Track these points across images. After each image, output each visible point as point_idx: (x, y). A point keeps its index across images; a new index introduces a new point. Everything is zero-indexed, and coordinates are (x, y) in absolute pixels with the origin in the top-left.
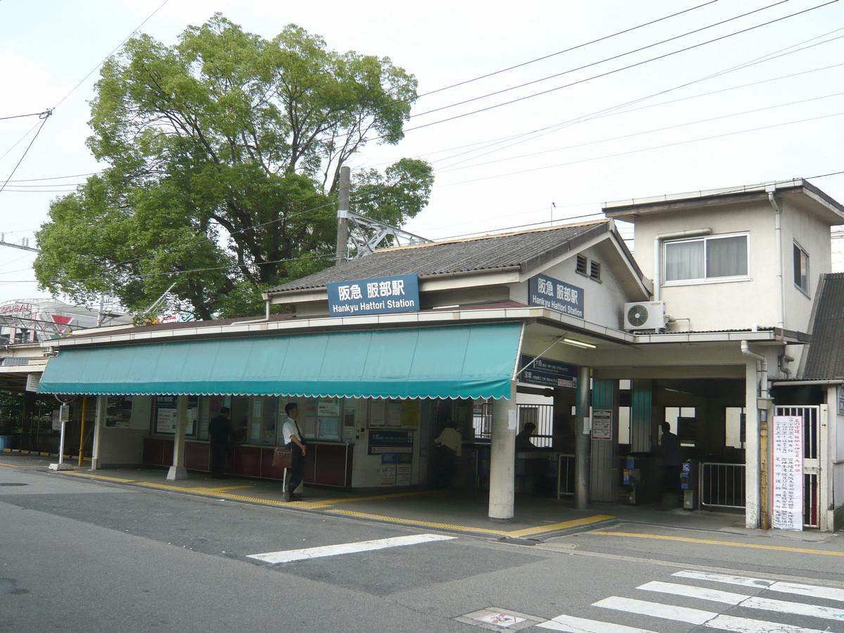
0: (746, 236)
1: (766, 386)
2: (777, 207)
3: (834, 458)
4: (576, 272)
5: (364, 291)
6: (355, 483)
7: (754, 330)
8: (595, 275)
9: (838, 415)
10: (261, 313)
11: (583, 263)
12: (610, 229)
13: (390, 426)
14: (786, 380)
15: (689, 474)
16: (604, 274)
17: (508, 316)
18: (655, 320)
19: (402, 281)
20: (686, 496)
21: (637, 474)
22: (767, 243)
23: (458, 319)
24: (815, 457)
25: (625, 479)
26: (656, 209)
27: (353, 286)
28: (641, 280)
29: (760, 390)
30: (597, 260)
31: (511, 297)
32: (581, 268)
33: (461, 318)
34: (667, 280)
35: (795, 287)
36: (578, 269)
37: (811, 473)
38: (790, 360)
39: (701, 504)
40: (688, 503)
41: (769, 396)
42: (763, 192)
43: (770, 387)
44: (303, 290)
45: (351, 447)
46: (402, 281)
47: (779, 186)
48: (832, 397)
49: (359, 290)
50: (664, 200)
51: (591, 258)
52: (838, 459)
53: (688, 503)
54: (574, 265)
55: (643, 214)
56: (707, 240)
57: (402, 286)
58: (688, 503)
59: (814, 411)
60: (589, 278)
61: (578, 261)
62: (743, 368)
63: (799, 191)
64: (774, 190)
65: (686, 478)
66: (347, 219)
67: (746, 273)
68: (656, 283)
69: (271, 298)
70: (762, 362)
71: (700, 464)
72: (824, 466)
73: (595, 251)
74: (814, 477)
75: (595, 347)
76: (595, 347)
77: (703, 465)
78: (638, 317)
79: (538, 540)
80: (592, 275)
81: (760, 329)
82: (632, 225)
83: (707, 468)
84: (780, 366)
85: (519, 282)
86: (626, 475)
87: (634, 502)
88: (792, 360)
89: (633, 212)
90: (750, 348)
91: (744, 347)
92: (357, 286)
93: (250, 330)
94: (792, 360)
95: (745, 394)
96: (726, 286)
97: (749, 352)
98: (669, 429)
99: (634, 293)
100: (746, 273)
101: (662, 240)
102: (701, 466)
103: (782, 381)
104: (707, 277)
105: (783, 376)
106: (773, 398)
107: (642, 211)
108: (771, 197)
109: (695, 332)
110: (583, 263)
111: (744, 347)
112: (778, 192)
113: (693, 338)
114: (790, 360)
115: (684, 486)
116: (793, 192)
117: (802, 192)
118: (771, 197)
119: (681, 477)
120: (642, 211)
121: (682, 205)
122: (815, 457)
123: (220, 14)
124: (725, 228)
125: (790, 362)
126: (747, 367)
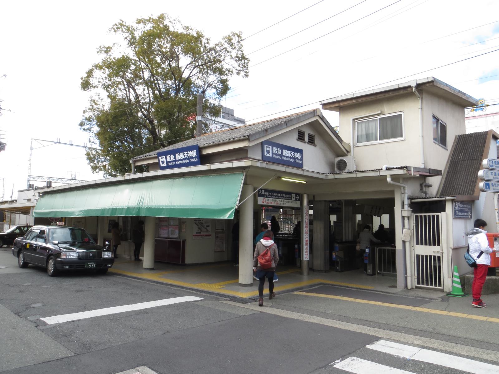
0: (401, 114)
1: (406, 202)
2: (419, 96)
3: (451, 246)
4: (297, 140)
5: (175, 157)
6: (188, 261)
7: (384, 169)
8: (312, 141)
9: (453, 218)
10: (130, 170)
11: (303, 135)
12: (318, 114)
13: (218, 230)
14: (425, 198)
15: (369, 254)
16: (317, 140)
17: (234, 166)
18: (351, 166)
19: (195, 151)
20: (368, 267)
21: (341, 254)
22: (415, 117)
23: (210, 169)
24: (439, 245)
25: (333, 257)
26: (348, 102)
27: (172, 155)
28: (341, 144)
29: (403, 205)
30: (312, 133)
31: (248, 155)
32: (301, 137)
33: (212, 168)
34: (358, 143)
35: (434, 142)
36: (298, 138)
37: (437, 255)
38: (429, 186)
39: (377, 271)
40: (369, 271)
41: (409, 208)
42: (409, 87)
43: (409, 203)
44: (148, 157)
45: (184, 242)
46: (195, 151)
47: (419, 82)
48: (449, 207)
49: (174, 157)
50: (353, 97)
51: (308, 132)
52: (454, 246)
53: (369, 271)
54: (296, 136)
55: (342, 106)
56: (379, 118)
57: (196, 153)
58: (369, 271)
59: (438, 216)
60: (307, 144)
61: (298, 133)
62: (393, 192)
63: (431, 84)
64: (416, 85)
65: (367, 257)
66: (201, 121)
67: (401, 136)
68: (351, 145)
69: (135, 162)
70: (404, 187)
71: (376, 248)
72: (445, 250)
73: (313, 130)
74: (439, 257)
75: (305, 182)
76: (305, 182)
77: (378, 249)
78: (342, 165)
79: (254, 300)
80: (309, 142)
81: (388, 169)
82: (337, 113)
83: (380, 250)
84: (422, 190)
85: (249, 146)
86: (334, 254)
87: (340, 270)
88: (431, 186)
89: (336, 105)
90: (392, 179)
91: (389, 179)
92: (173, 155)
93: (118, 180)
94: (431, 186)
95: (394, 206)
96: (391, 144)
97: (392, 182)
98: (384, 227)
99: (337, 151)
100: (401, 136)
101: (354, 120)
102: (377, 249)
103: (423, 198)
104: (379, 140)
105: (424, 195)
106: (412, 210)
107: (342, 104)
108: (414, 89)
109: (360, 171)
110: (303, 135)
111: (389, 179)
112: (419, 86)
113: (359, 175)
114: (429, 186)
115: (366, 261)
116: (428, 85)
117: (433, 85)
118: (414, 89)
119: (364, 256)
120: (342, 104)
121: (364, 99)
122: (439, 245)
123: (209, 40)
124: (389, 110)
125: (430, 187)
126: (395, 191)
